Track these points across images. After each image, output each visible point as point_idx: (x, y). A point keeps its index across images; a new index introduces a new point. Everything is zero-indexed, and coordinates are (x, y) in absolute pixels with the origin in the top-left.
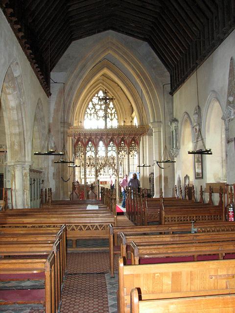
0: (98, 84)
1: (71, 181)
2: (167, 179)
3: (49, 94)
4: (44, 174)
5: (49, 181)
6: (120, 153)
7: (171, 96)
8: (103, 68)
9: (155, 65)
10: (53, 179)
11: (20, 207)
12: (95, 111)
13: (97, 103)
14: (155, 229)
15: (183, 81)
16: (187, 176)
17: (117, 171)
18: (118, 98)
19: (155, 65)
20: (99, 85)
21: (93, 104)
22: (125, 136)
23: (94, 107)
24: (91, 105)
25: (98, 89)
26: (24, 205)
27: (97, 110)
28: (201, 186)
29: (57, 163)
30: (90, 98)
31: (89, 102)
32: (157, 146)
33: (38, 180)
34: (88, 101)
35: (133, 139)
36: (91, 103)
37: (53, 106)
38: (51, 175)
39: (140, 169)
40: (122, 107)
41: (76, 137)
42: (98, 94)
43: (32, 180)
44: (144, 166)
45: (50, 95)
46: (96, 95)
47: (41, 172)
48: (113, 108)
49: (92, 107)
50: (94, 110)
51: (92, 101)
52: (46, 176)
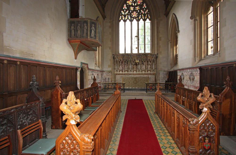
21: (127, 6)
24: (125, 7)
36: (125, 5)
48: (146, 9)
49: (126, 8)
51: (126, 4)
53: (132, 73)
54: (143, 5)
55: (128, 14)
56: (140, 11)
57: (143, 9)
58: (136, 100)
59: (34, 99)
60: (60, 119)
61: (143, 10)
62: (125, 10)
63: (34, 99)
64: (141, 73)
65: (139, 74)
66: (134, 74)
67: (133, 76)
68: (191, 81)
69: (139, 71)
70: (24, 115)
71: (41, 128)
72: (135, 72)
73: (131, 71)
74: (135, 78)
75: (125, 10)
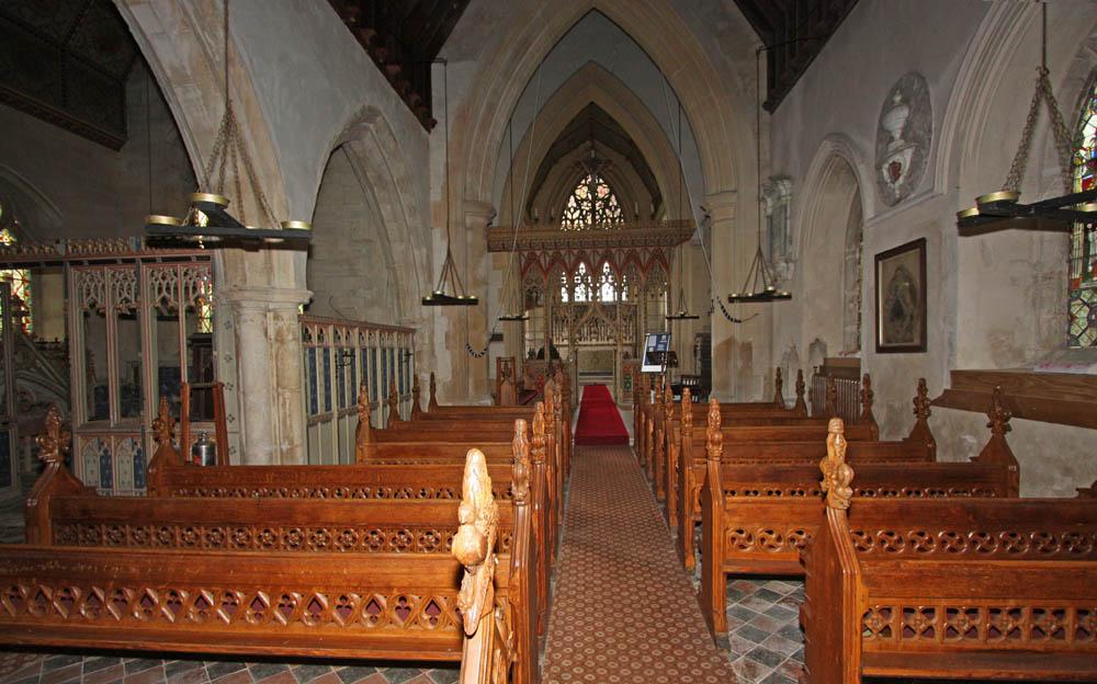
2: (751, 349)
3: (429, 123)
4: (422, 337)
5: (436, 353)
9: (721, 26)
10: (447, 348)
11: (259, 458)
12: (581, 214)
15: (809, 56)
16: (817, 340)
19: (721, 26)
21: (576, 200)
24: (572, 203)
26: (271, 458)
27: (584, 212)
29: (757, 298)
33: (396, 353)
36: (572, 198)
37: (438, 159)
38: (440, 339)
39: (680, 325)
43: (404, 352)
47: (413, 331)
48: (616, 208)
49: (575, 205)
50: (578, 212)
51: (575, 195)
52: (427, 341)
53: (588, 342)
54: (609, 200)
55: (578, 218)
56: (604, 213)
57: (610, 208)
58: (595, 384)
59: (296, 595)
60: (24, 337)
61: (610, 209)
62: (572, 210)
63: (296, 595)
64: (606, 342)
65: (603, 345)
66: (591, 345)
67: (589, 349)
68: (432, 376)
69: (603, 339)
70: (607, 294)
71: (1006, 496)
72: (594, 342)
73: (586, 339)
74: (595, 354)
75: (572, 210)
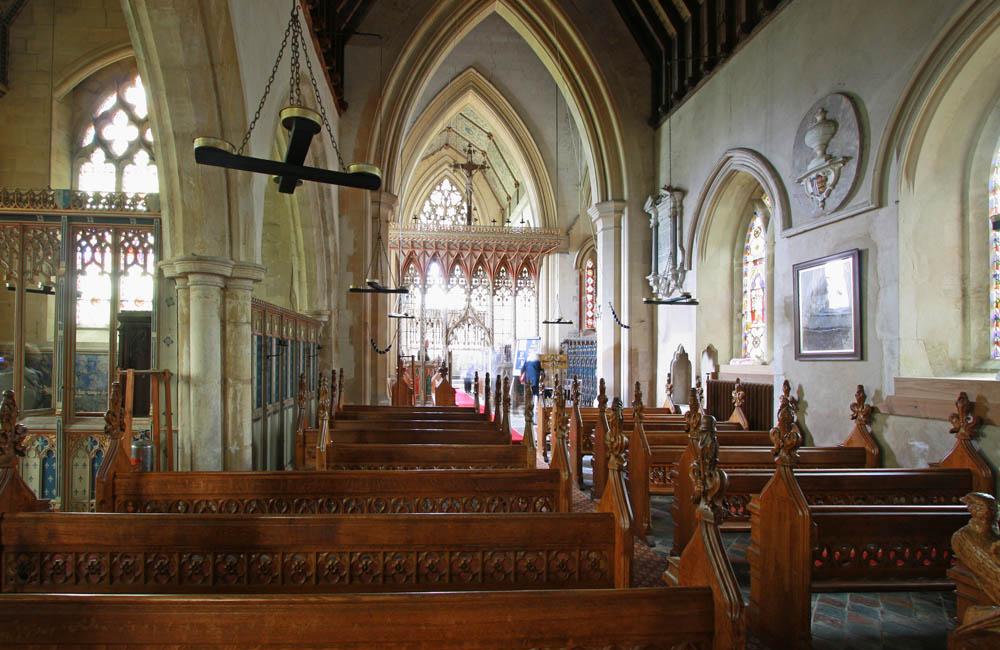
0: (441, 166)
1: (392, 356)
6: (498, 292)
7: (650, 129)
8: (465, 91)
13: (439, 203)
14: (892, 617)
17: (490, 333)
18: (478, 193)
20: (444, 168)
21: (431, 205)
22: (511, 253)
23: (434, 211)
25: (441, 176)
27: (438, 218)
28: (861, 388)
30: (425, 194)
31: (424, 202)
32: (611, 265)
34: (423, 198)
35: (527, 263)
36: (427, 203)
40: (485, 212)
41: (406, 252)
42: (441, 185)
44: (559, 322)
45: (345, 109)
46: (438, 188)
51: (430, 200)
